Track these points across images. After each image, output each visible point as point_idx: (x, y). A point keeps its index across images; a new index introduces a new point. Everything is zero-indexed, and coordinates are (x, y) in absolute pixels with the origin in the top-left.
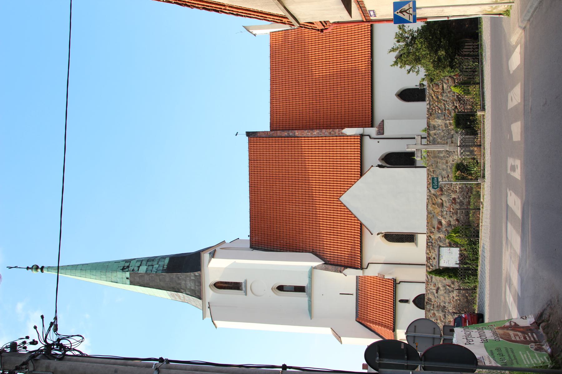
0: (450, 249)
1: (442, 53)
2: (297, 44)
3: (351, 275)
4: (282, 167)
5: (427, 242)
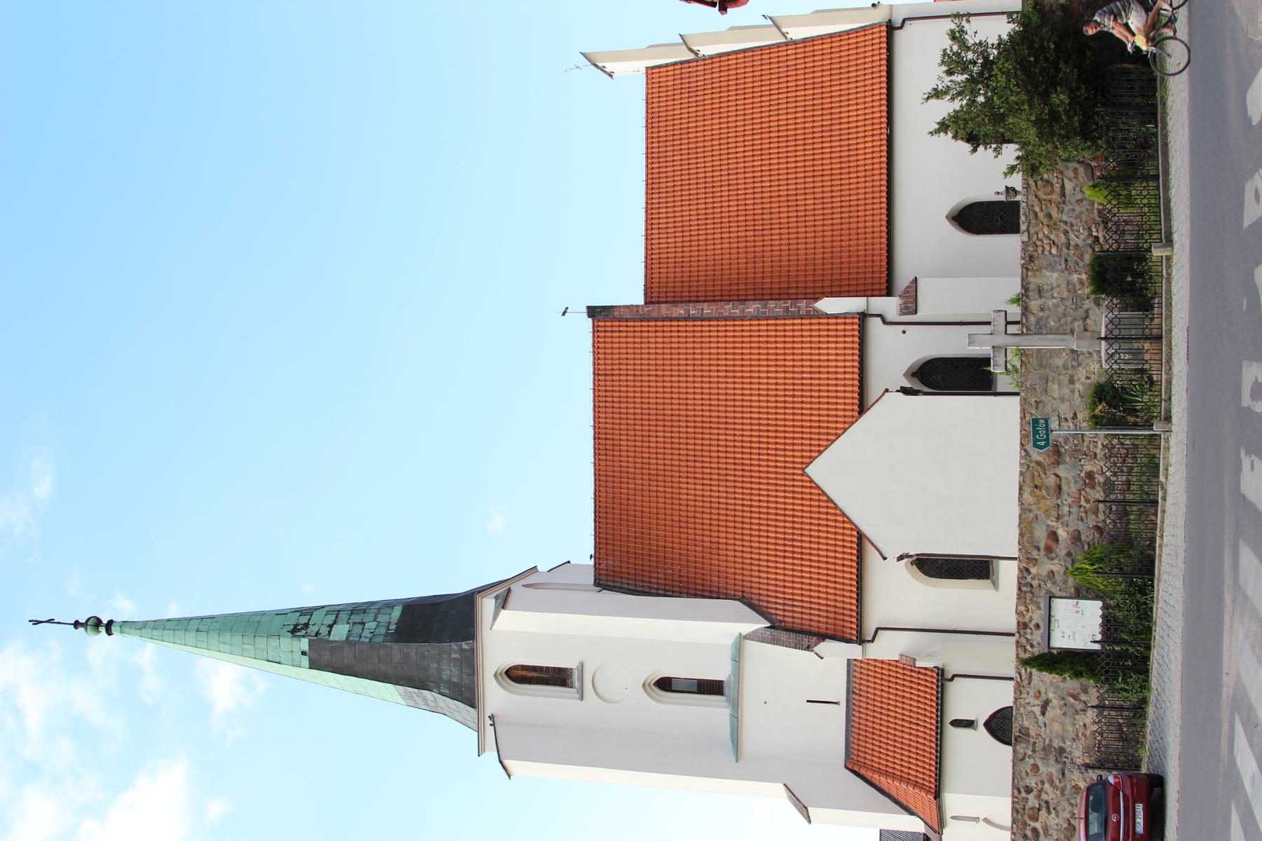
0: (1077, 603)
1: (1060, 98)
2: (710, 97)
3: (836, 655)
4: (672, 393)
5: (1019, 584)
